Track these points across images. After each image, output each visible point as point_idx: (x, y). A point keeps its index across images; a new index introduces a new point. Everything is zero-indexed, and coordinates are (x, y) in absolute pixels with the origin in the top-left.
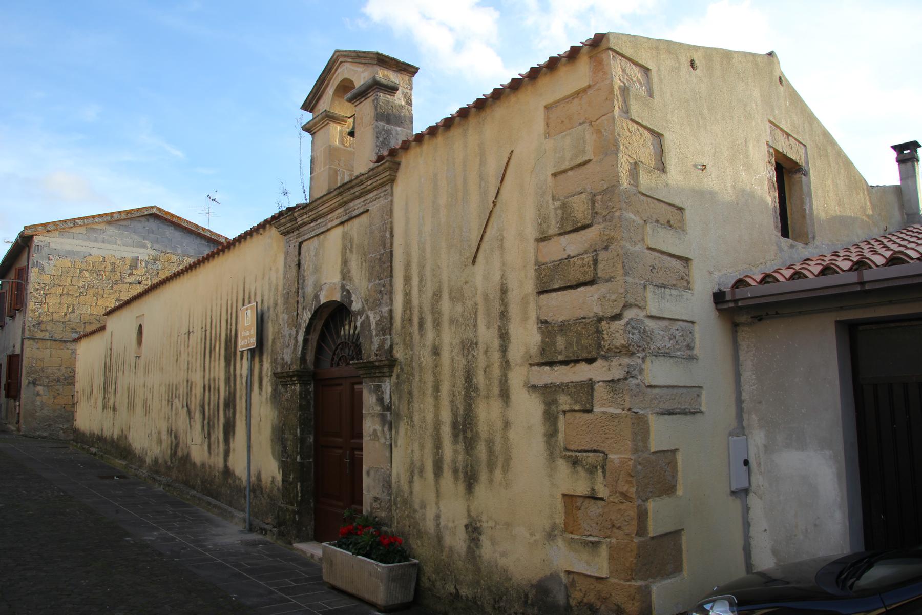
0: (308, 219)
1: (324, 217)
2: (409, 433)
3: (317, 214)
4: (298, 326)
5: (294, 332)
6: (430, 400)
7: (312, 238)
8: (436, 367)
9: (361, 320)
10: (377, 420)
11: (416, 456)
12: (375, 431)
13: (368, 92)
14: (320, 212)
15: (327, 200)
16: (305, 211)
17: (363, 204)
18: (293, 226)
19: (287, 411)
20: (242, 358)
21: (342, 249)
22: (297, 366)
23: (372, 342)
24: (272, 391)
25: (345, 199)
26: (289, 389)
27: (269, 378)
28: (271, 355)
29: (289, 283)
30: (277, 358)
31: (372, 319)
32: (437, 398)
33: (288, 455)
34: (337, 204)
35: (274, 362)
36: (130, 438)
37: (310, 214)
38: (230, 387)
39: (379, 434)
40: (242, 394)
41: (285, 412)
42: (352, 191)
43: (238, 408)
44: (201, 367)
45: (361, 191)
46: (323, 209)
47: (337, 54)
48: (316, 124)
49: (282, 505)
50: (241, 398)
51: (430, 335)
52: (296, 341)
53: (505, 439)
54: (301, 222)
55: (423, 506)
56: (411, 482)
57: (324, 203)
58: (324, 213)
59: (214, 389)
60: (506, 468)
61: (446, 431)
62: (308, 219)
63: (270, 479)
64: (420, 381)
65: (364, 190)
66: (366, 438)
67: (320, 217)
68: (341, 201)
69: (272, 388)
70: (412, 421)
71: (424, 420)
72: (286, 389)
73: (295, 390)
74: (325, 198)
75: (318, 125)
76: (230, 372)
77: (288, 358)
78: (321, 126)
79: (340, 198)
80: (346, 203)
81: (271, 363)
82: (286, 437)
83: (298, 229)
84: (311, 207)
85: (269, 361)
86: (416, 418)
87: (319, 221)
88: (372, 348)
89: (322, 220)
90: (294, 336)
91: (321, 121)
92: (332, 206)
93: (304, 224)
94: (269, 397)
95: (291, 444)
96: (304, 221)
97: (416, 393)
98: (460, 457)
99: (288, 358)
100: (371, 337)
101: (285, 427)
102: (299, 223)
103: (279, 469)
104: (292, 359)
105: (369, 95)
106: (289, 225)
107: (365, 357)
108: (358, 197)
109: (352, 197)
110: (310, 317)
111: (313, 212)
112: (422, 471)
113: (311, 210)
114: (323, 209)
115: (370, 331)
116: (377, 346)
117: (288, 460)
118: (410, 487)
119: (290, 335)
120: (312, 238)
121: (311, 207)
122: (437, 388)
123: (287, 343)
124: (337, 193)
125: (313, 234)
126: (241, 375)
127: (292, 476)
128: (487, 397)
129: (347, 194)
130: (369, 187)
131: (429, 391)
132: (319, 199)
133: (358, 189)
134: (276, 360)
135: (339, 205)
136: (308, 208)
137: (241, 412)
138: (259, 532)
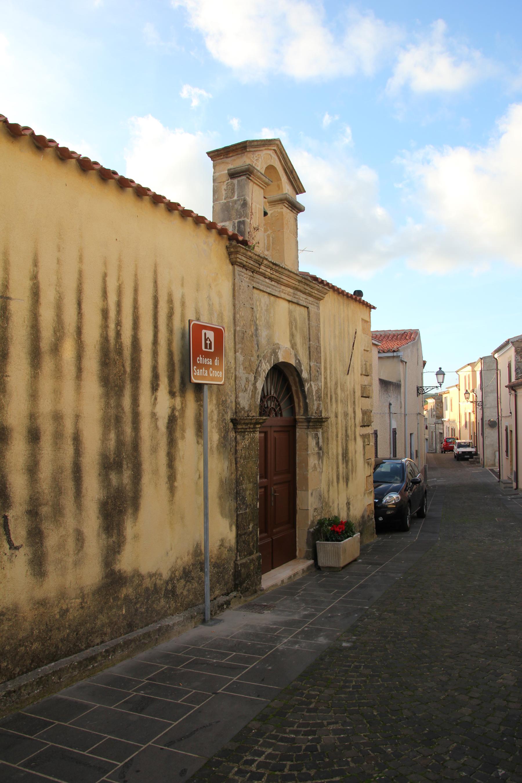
0: (269, 274)
1: (278, 283)
2: (327, 463)
3: (279, 279)
4: (257, 373)
5: (252, 377)
6: (335, 442)
7: (263, 291)
8: (337, 424)
9: (308, 387)
10: (316, 456)
11: (330, 476)
12: (315, 464)
13: (214, 154)
14: (282, 280)
15: (291, 277)
16: (274, 267)
17: (304, 299)
18: (254, 267)
19: (244, 460)
20: (155, 388)
21: (289, 323)
22: (256, 413)
23: (314, 404)
24: (219, 439)
25: (299, 287)
26: (246, 437)
27: (214, 423)
28: (217, 396)
29: (244, 322)
30: (226, 401)
31: (313, 387)
32: (337, 441)
33: (247, 506)
34: (294, 285)
35: (222, 404)
36: (140, 571)
37: (274, 273)
38: (120, 434)
39: (317, 466)
40: (157, 444)
41: (242, 461)
42: (306, 287)
43: (147, 466)
44: (502, 433)
45: (310, 292)
46: (285, 279)
47: (278, 143)
48: (259, 178)
49: (244, 561)
50: (154, 450)
51: (334, 406)
52: (255, 388)
53: (355, 458)
54: (263, 271)
55: (333, 503)
56: (328, 491)
57: (288, 276)
58: (282, 282)
59: (58, 436)
60: (356, 472)
61: (340, 457)
62: (269, 274)
63: (219, 543)
64: (331, 432)
65: (311, 293)
66: (310, 470)
67: (278, 282)
68: (297, 286)
69: (220, 435)
70: (329, 455)
71: (333, 454)
72: (244, 437)
73: (253, 438)
74: (292, 275)
75: (258, 180)
76: (119, 406)
77: (245, 402)
78: (259, 184)
79: (297, 283)
80: (297, 289)
81: (218, 405)
82: (244, 488)
83: (253, 272)
84: (280, 270)
85: (214, 402)
86: (330, 453)
87: (273, 283)
88: (314, 408)
89: (276, 284)
90: (253, 382)
91: (262, 182)
92: (291, 284)
93: (264, 275)
94: (215, 446)
95: (250, 494)
96: (267, 273)
97: (330, 438)
98: (345, 471)
99: (245, 402)
100: (313, 401)
101: (243, 477)
102: (261, 270)
103: (231, 526)
104: (250, 405)
105: (294, 211)
106: (252, 263)
107: (310, 414)
108: (304, 293)
109: (302, 289)
110: (269, 368)
111: (277, 274)
112: (332, 483)
113: (277, 271)
114: (285, 279)
115: (312, 396)
116: (316, 407)
117: (247, 510)
118: (328, 494)
119: (247, 380)
120: (263, 291)
121: (280, 270)
122: (337, 437)
123: (243, 386)
124: (300, 280)
125: (268, 290)
126: (154, 415)
127: (251, 526)
128: (351, 440)
129: (302, 285)
130: (314, 294)
131: (335, 438)
132: (289, 271)
133: (309, 289)
134: (224, 403)
135: (294, 287)
136: (277, 268)
137: (155, 472)
138: (218, 612)
